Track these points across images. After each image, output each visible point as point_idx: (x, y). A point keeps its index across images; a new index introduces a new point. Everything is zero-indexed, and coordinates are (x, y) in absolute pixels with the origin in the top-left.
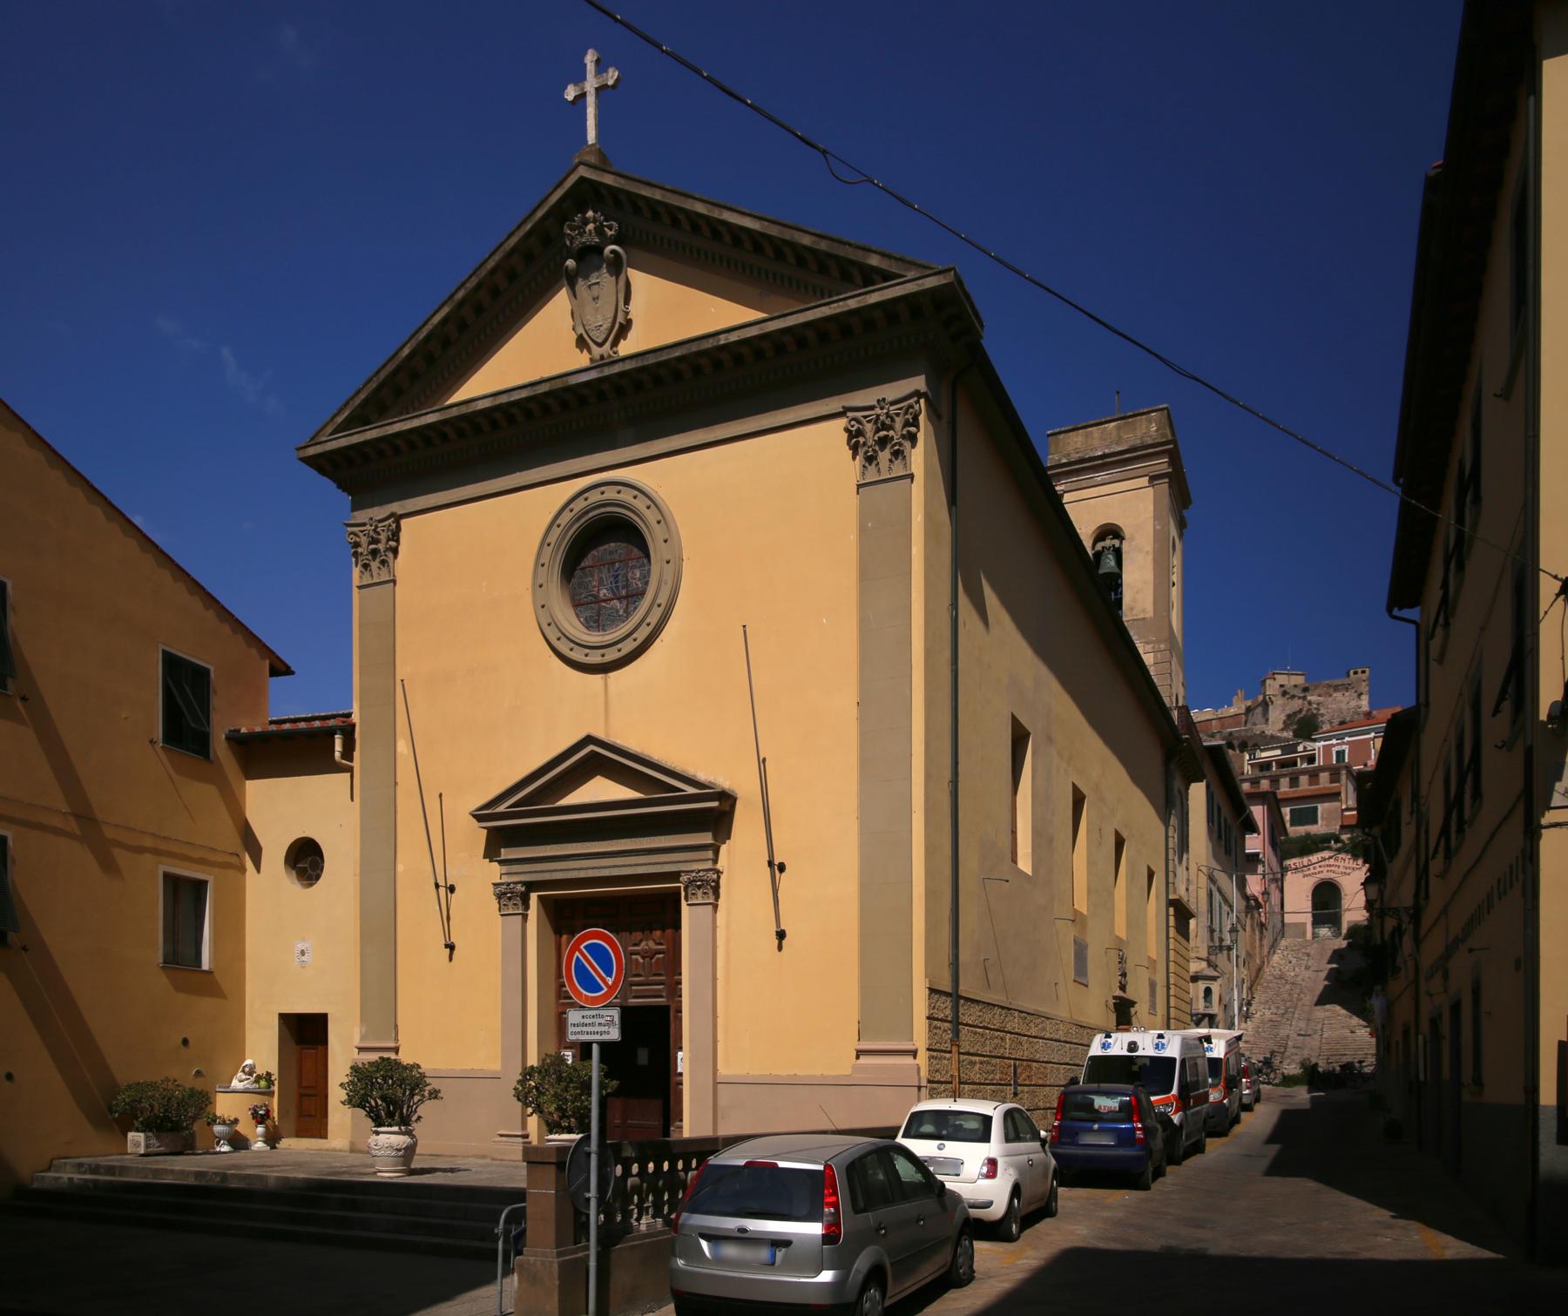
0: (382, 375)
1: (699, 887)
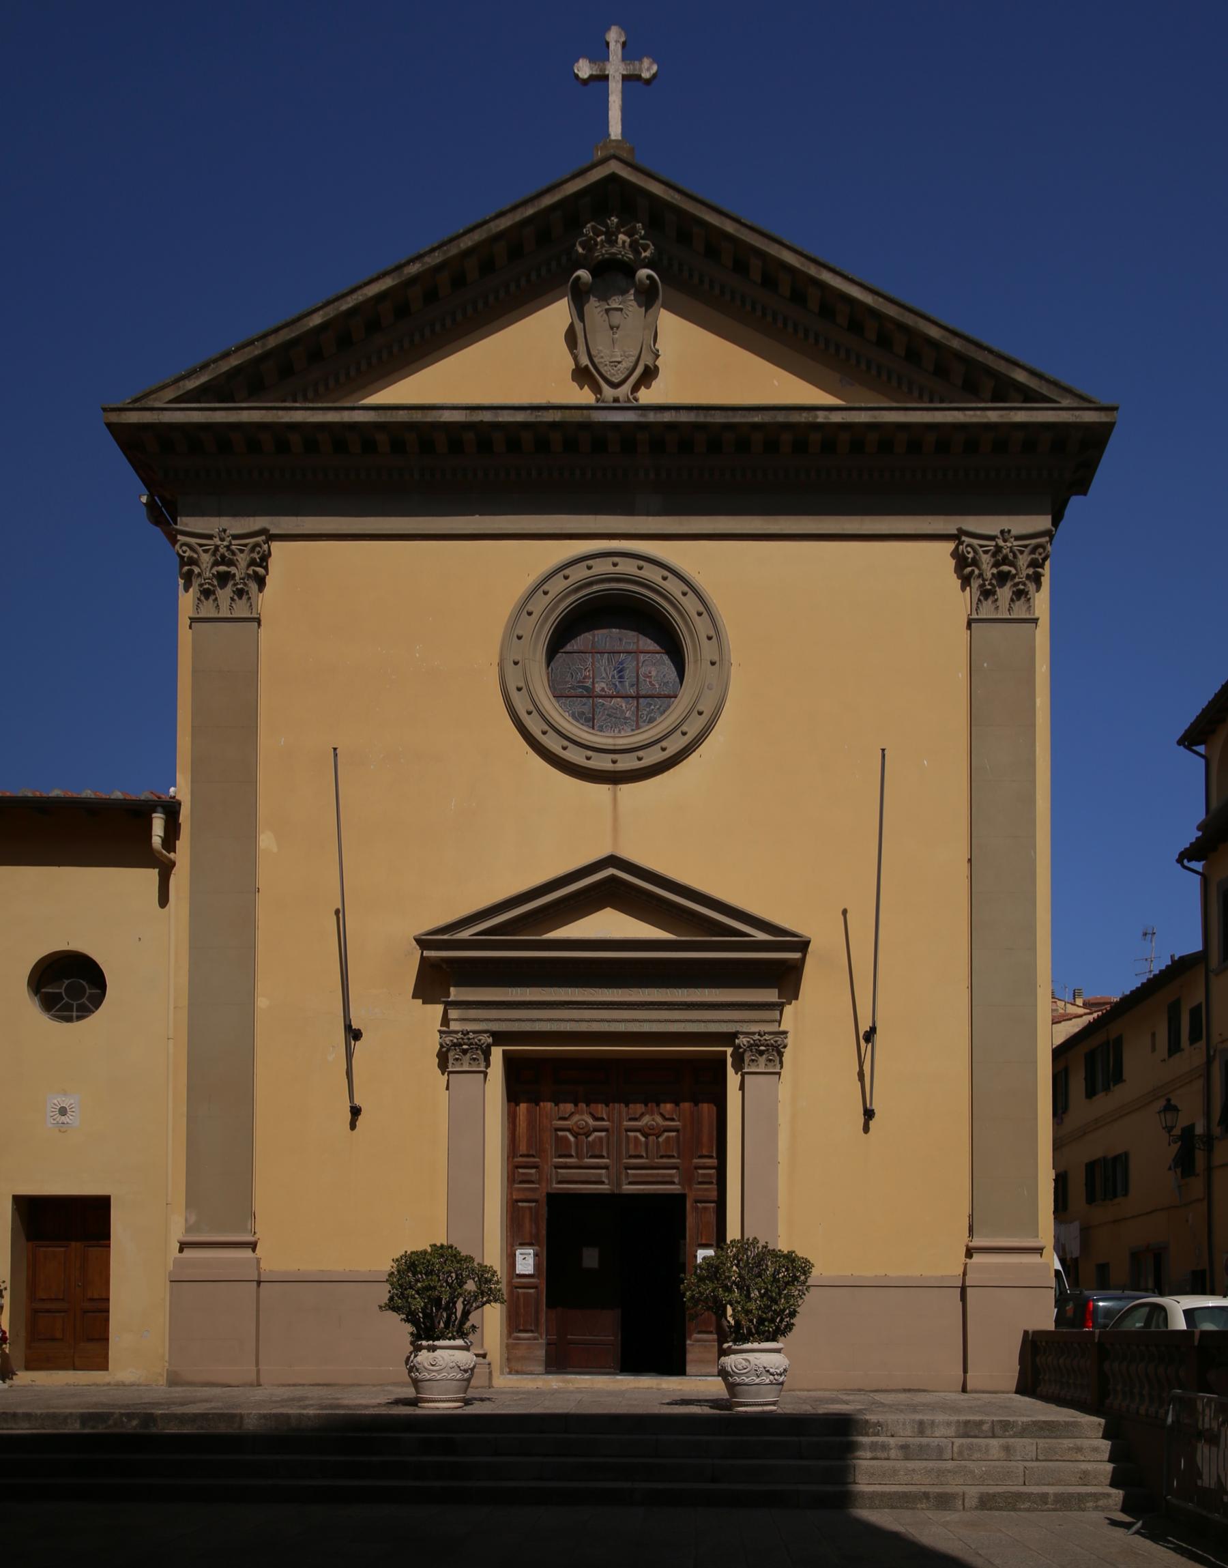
0: (272, 342)
1: (761, 1053)
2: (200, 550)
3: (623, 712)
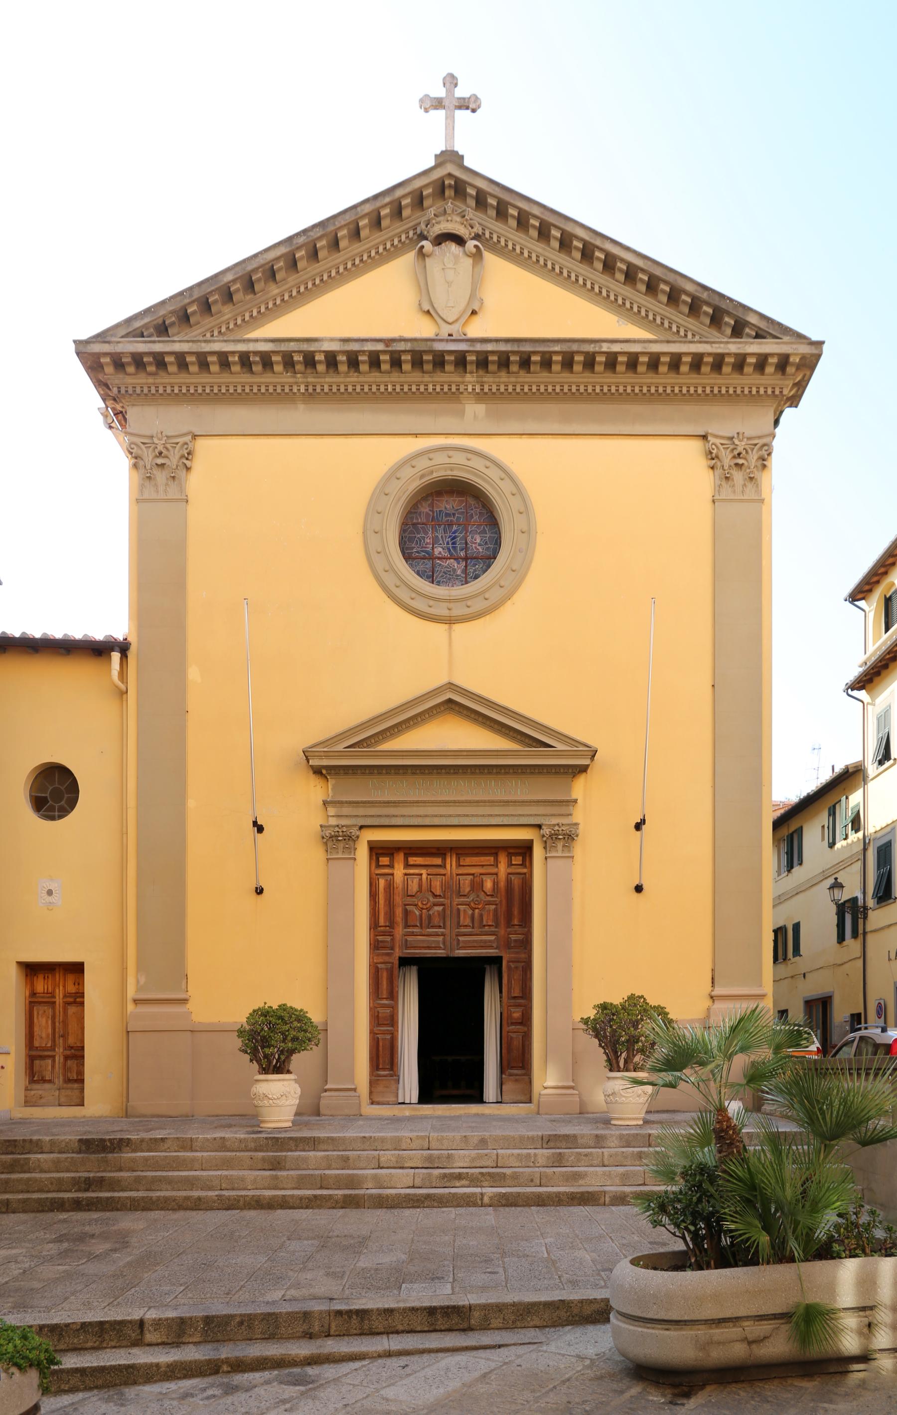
2: (143, 446)
3: (454, 570)
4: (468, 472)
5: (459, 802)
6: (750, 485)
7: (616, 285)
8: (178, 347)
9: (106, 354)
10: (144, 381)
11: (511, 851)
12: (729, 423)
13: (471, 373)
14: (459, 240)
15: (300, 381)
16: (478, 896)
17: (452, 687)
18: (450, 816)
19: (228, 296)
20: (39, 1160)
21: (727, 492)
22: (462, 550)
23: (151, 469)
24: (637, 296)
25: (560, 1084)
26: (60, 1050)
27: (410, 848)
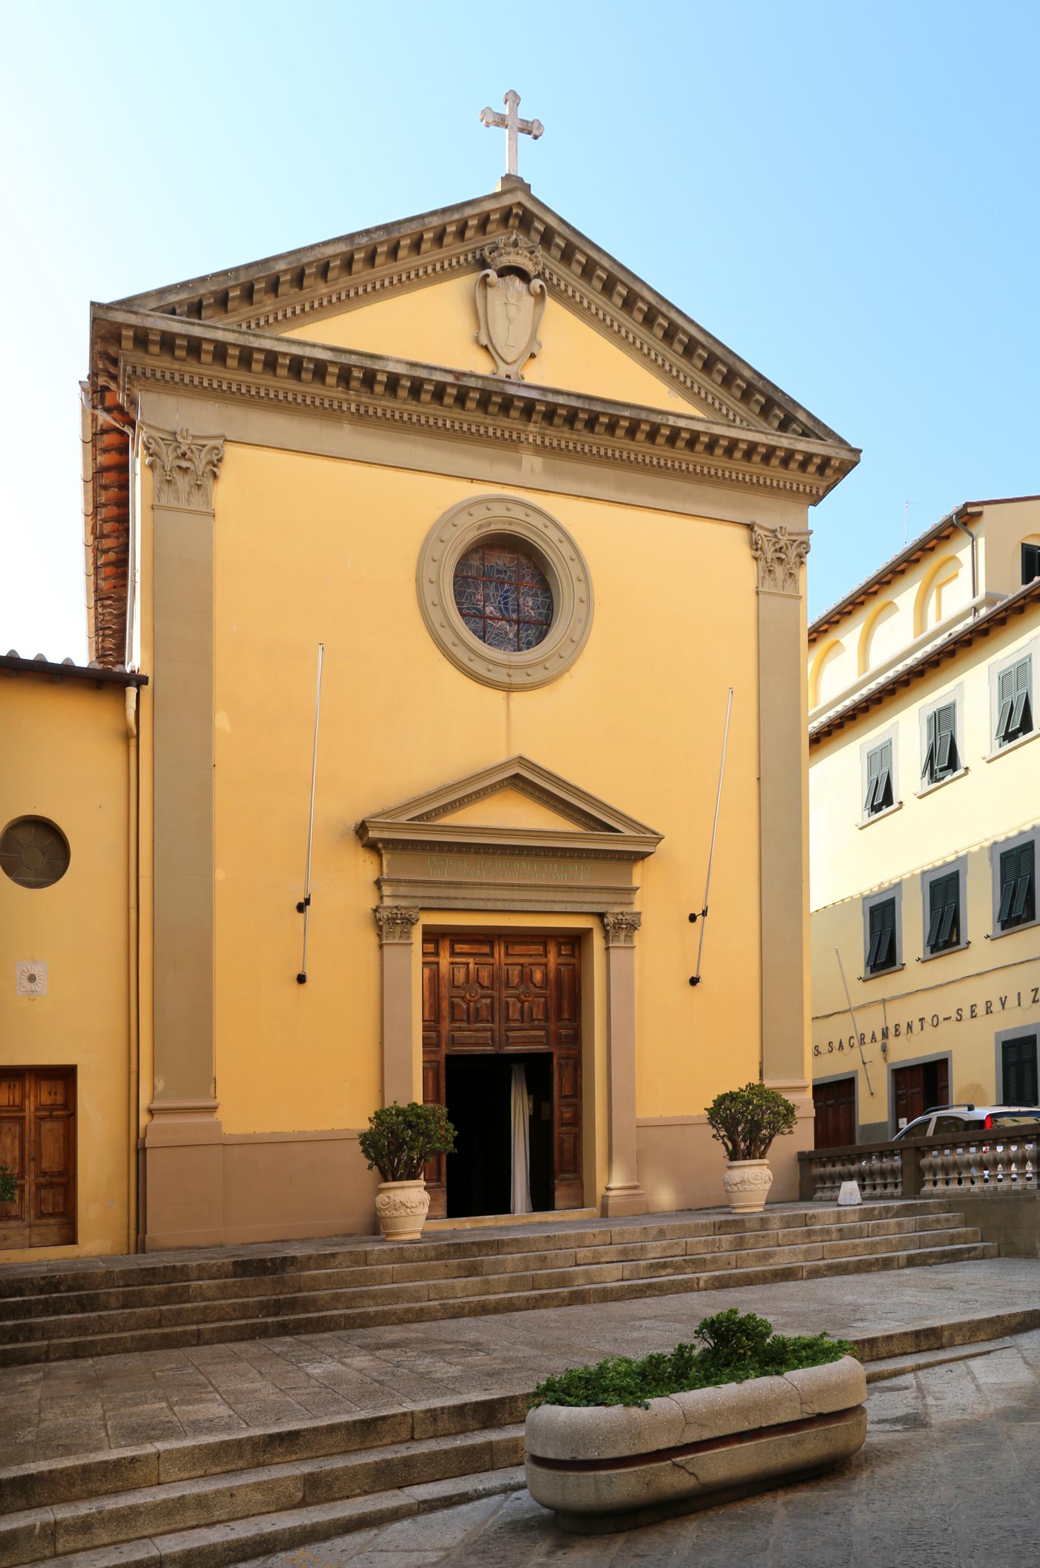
2: (161, 443)
3: (507, 633)
4: (528, 529)
5: (523, 886)
6: (789, 581)
7: (673, 356)
8: (220, 336)
9: (129, 326)
10: (168, 365)
11: (561, 940)
12: (771, 516)
13: (535, 422)
14: (524, 275)
15: (353, 398)
16: (528, 988)
17: (522, 761)
18: (513, 900)
19: (274, 286)
20: (201, 1287)
21: (769, 586)
22: (514, 612)
23: (171, 471)
24: (692, 371)
25: (626, 1185)
26: (30, 1178)
27: (456, 934)
